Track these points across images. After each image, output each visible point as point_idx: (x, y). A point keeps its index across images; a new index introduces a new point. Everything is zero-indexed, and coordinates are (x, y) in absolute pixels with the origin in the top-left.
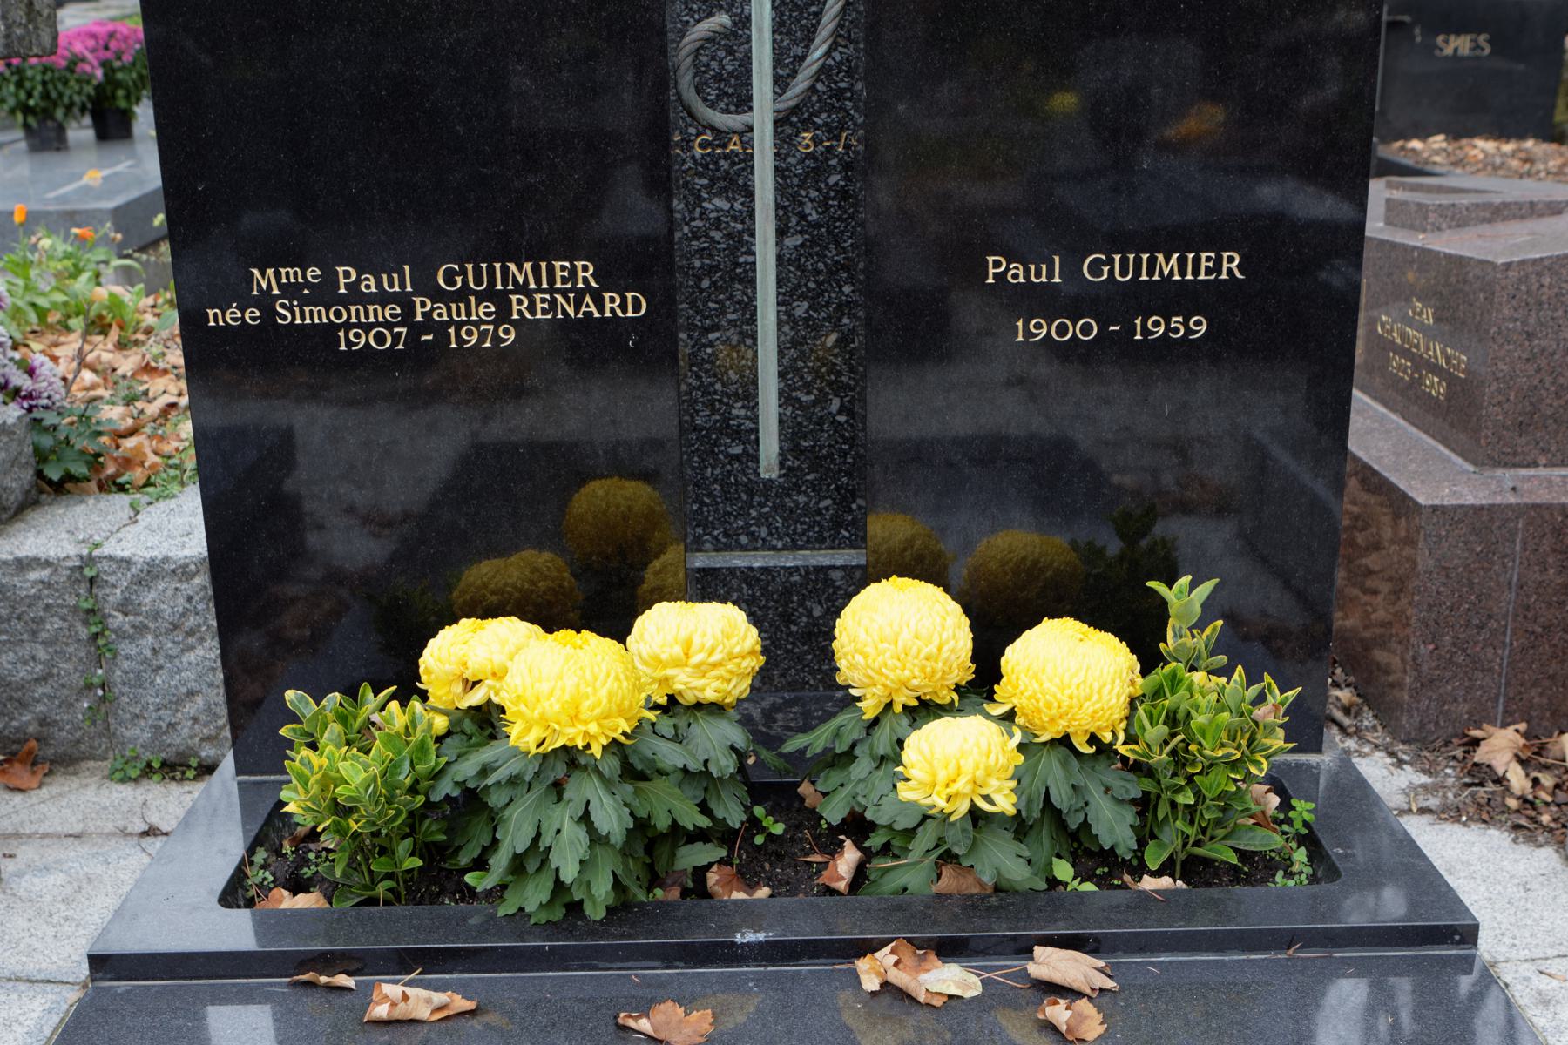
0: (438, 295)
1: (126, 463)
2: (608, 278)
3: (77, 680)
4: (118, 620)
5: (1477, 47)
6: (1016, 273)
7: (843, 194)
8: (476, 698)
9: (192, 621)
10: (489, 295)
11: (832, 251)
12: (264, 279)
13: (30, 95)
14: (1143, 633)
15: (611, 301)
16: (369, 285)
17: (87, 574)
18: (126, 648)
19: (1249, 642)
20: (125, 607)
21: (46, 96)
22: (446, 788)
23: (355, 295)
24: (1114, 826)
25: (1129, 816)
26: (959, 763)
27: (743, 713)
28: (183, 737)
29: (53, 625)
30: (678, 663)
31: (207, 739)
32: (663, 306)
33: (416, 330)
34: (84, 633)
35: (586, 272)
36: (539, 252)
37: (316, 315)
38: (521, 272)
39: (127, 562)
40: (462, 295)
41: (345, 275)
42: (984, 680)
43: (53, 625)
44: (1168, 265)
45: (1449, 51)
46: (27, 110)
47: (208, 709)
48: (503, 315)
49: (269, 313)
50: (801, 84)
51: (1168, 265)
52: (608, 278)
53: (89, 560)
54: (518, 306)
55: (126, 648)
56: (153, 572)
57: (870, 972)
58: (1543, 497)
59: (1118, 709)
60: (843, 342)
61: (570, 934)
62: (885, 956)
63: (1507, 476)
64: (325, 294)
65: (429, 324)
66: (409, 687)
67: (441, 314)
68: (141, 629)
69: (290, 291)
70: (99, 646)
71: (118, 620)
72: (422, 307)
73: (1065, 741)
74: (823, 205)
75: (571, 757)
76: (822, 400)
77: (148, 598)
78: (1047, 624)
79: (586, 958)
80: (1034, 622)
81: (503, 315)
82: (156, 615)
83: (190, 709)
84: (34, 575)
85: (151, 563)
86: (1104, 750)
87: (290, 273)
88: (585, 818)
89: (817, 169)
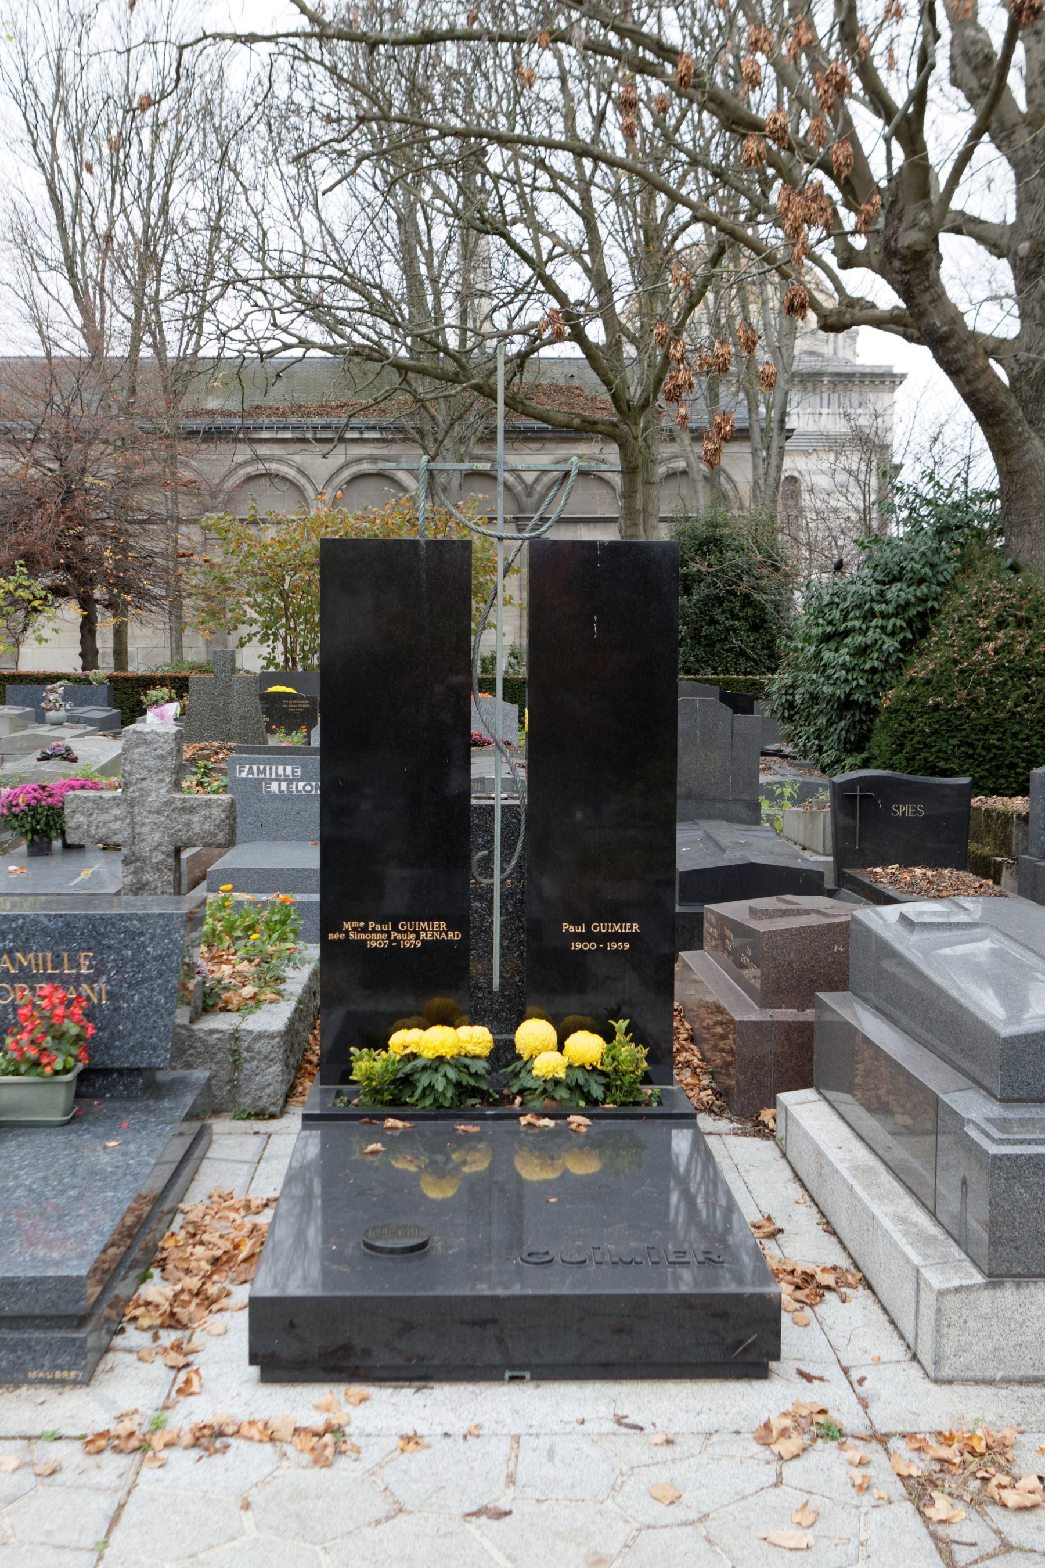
0: (399, 931)
1: (227, 1002)
2: (450, 928)
3: (226, 1078)
4: (245, 1054)
5: (917, 811)
6: (571, 929)
7: (522, 902)
8: (408, 1051)
9: (272, 1056)
10: (414, 932)
11: (517, 922)
12: (347, 925)
13: (38, 823)
14: (608, 1036)
15: (451, 934)
16: (378, 928)
17: (235, 1036)
18: (246, 1066)
19: (637, 1035)
20: (248, 1049)
21: (47, 824)
22: (400, 1075)
23: (374, 931)
24: (597, 1092)
25: (602, 1088)
26: (548, 1064)
27: (488, 1059)
28: (264, 1102)
29: (220, 1055)
30: (469, 1042)
31: (273, 1104)
32: (466, 936)
33: (391, 942)
34: (231, 1059)
35: (443, 925)
36: (430, 919)
37: (362, 936)
38: (424, 925)
39: (251, 1032)
40: (406, 931)
41: (371, 925)
42: (561, 1048)
43: (220, 1055)
44: (617, 927)
45: (899, 813)
46: (34, 831)
47: (275, 1091)
48: (418, 938)
49: (347, 935)
50: (508, 871)
51: (617, 927)
52: (450, 928)
53: (237, 1031)
54: (423, 935)
55: (246, 1066)
56: (261, 1036)
57: (523, 1121)
58: (782, 1018)
59: (599, 1056)
60: (521, 955)
61: (440, 1112)
62: (529, 1117)
63: (770, 1011)
64: (364, 930)
65: (395, 940)
66: (386, 1048)
67: (399, 937)
68: (253, 1058)
69: (354, 929)
70: (236, 1066)
71: (245, 1054)
72: (394, 934)
73: (582, 1067)
74: (514, 906)
75: (440, 1059)
76: (512, 977)
77: (257, 1046)
78: (579, 1032)
79: (444, 1117)
80: (575, 1031)
81: (418, 938)
82: (259, 1052)
83: (268, 1091)
84: (215, 1036)
85: (260, 1032)
86: (594, 1068)
87: (355, 924)
88: (445, 1076)
89: (512, 894)
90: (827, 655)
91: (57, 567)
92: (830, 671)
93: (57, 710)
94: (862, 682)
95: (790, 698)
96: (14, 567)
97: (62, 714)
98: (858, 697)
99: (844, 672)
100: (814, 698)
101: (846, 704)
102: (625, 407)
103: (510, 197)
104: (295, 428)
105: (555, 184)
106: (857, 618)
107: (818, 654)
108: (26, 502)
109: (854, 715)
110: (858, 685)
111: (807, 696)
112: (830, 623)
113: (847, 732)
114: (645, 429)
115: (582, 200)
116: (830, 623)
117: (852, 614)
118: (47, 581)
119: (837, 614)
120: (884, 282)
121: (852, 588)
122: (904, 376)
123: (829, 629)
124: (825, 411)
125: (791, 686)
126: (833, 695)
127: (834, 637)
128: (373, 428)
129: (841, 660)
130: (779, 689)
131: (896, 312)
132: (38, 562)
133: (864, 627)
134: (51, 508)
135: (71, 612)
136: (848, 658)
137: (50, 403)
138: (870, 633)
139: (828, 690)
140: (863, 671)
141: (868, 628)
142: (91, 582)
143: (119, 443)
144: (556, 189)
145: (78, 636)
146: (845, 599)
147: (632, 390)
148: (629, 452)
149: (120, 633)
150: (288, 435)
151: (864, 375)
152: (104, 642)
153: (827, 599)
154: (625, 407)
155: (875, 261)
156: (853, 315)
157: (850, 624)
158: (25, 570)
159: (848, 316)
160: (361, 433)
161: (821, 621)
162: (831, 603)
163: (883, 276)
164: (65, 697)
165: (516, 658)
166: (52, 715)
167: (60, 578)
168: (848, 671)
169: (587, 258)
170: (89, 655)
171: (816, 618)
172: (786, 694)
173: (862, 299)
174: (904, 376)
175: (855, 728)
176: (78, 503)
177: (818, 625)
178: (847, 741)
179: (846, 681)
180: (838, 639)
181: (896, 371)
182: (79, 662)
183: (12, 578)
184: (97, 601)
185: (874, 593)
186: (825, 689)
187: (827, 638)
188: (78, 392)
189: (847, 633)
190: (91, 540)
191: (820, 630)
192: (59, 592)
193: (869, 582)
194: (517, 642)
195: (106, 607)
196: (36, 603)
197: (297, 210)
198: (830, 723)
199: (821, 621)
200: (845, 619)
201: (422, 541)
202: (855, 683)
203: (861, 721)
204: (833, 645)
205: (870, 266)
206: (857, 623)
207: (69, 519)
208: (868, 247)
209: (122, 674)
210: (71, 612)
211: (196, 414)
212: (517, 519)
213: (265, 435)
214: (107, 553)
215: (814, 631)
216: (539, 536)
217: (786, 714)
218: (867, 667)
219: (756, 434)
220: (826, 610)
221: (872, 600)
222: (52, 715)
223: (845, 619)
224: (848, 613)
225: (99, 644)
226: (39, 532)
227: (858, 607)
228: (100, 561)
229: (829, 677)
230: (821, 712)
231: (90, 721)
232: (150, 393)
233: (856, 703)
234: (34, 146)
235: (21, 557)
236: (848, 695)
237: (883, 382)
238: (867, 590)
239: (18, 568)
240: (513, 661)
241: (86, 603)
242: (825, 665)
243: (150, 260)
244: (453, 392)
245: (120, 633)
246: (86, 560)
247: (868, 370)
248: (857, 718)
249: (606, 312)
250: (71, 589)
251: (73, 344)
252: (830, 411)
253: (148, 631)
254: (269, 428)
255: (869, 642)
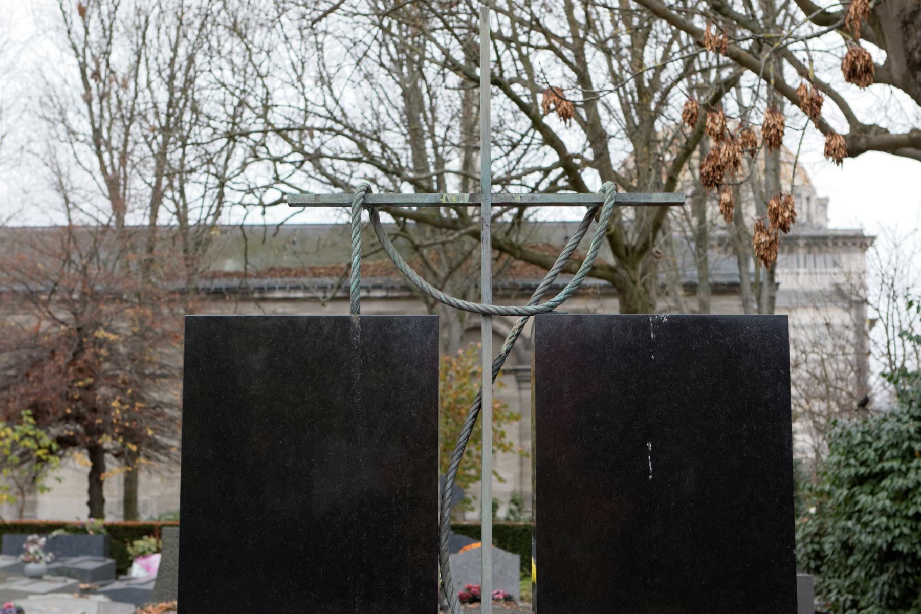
90: (864, 499)
91: (66, 418)
92: (866, 518)
93: (37, 562)
94: (906, 530)
95: (816, 547)
96: (21, 417)
97: (42, 566)
98: (903, 547)
99: (884, 519)
100: (848, 548)
101: (888, 556)
102: (623, 252)
103: (506, 56)
104: (306, 289)
105: (549, 42)
106: (893, 458)
107: (851, 497)
108: (34, 357)
109: (897, 567)
110: (901, 534)
111: (838, 546)
112: (863, 463)
113: (891, 586)
114: (643, 274)
115: (577, 57)
116: (863, 463)
117: (888, 454)
118: (54, 431)
119: (871, 454)
120: (907, 97)
121: (887, 426)
122: (873, 238)
123: (862, 470)
124: (802, 270)
125: (816, 534)
126: (873, 545)
127: (871, 479)
128: (378, 287)
129: (879, 505)
130: (804, 538)
131: (915, 135)
132: (48, 413)
133: (903, 468)
134: (62, 362)
135: (78, 463)
136: (888, 503)
137: (68, 261)
138: (912, 475)
139: (867, 539)
140: (906, 517)
141: (908, 469)
142: (100, 432)
143: (136, 300)
144: (550, 47)
145: (86, 485)
146: (879, 438)
147: (630, 235)
148: (628, 296)
149: (130, 483)
150: (300, 294)
151: (836, 238)
152: (113, 492)
153: (859, 437)
154: (623, 252)
155: (897, 76)
156: (868, 140)
157: (887, 465)
158: (31, 420)
159: (863, 140)
160: (369, 291)
161: (852, 461)
162: (863, 442)
163: (906, 90)
164: (46, 549)
165: (517, 504)
166: (31, 567)
167: (68, 429)
168: (889, 517)
169: (583, 113)
170: (96, 504)
171: (847, 459)
172: (812, 542)
173: (875, 125)
174: (873, 238)
175: (899, 582)
176: (88, 355)
177: (848, 465)
178: (890, 596)
179: (887, 529)
180: (874, 482)
181: (866, 233)
182: (87, 510)
183: (18, 427)
184: (107, 451)
185: (912, 430)
186: (863, 537)
187: (859, 481)
188: (94, 254)
189: (883, 474)
190: (103, 391)
191: (853, 471)
192: (65, 443)
193: (905, 418)
194: (518, 488)
195: (116, 456)
196: (40, 453)
197: (299, 70)
198: (869, 576)
199: (852, 461)
200: (881, 458)
201: (356, 320)
202: (897, 532)
203: (905, 574)
204: (867, 487)
205: (890, 81)
206: (896, 464)
207: (80, 370)
208: (888, 61)
209: (130, 523)
210: (78, 463)
211: (215, 275)
212: (517, 371)
213: (279, 294)
214: (115, 404)
215: (845, 473)
216: (550, 310)
217: (812, 565)
218: (911, 512)
219: (747, 288)
220: (858, 450)
221: (910, 438)
222: (31, 567)
223: (881, 458)
224: (883, 453)
225: (106, 494)
226: (51, 381)
227: (895, 445)
228: (108, 411)
229: (866, 525)
230: (858, 563)
231: (81, 575)
232: (171, 258)
233: (899, 554)
234: (69, 32)
235: (30, 407)
236: (891, 545)
237: (854, 244)
238: (904, 427)
239: (25, 418)
240: (514, 507)
241: (96, 454)
242: (859, 511)
243: (171, 130)
244: (451, 238)
245: (130, 483)
246: (95, 410)
247: (840, 233)
248: (901, 571)
249: (602, 162)
250: (78, 440)
251: (94, 209)
252: (807, 270)
253: (156, 480)
254: (282, 288)
255: (911, 485)
